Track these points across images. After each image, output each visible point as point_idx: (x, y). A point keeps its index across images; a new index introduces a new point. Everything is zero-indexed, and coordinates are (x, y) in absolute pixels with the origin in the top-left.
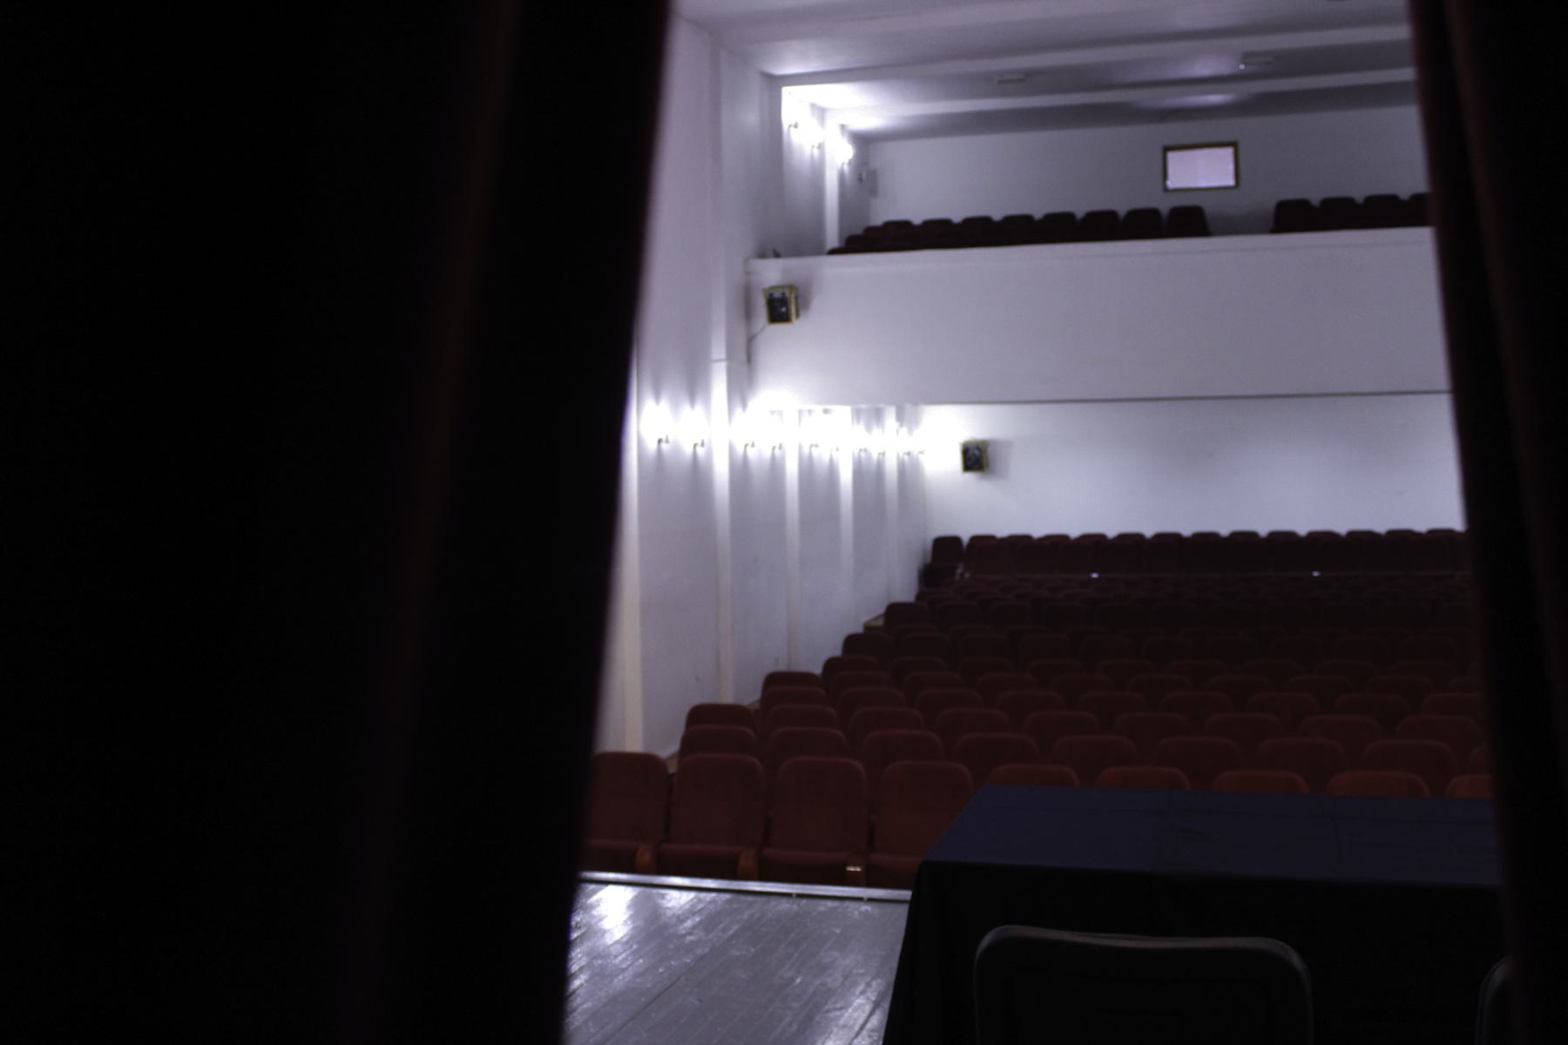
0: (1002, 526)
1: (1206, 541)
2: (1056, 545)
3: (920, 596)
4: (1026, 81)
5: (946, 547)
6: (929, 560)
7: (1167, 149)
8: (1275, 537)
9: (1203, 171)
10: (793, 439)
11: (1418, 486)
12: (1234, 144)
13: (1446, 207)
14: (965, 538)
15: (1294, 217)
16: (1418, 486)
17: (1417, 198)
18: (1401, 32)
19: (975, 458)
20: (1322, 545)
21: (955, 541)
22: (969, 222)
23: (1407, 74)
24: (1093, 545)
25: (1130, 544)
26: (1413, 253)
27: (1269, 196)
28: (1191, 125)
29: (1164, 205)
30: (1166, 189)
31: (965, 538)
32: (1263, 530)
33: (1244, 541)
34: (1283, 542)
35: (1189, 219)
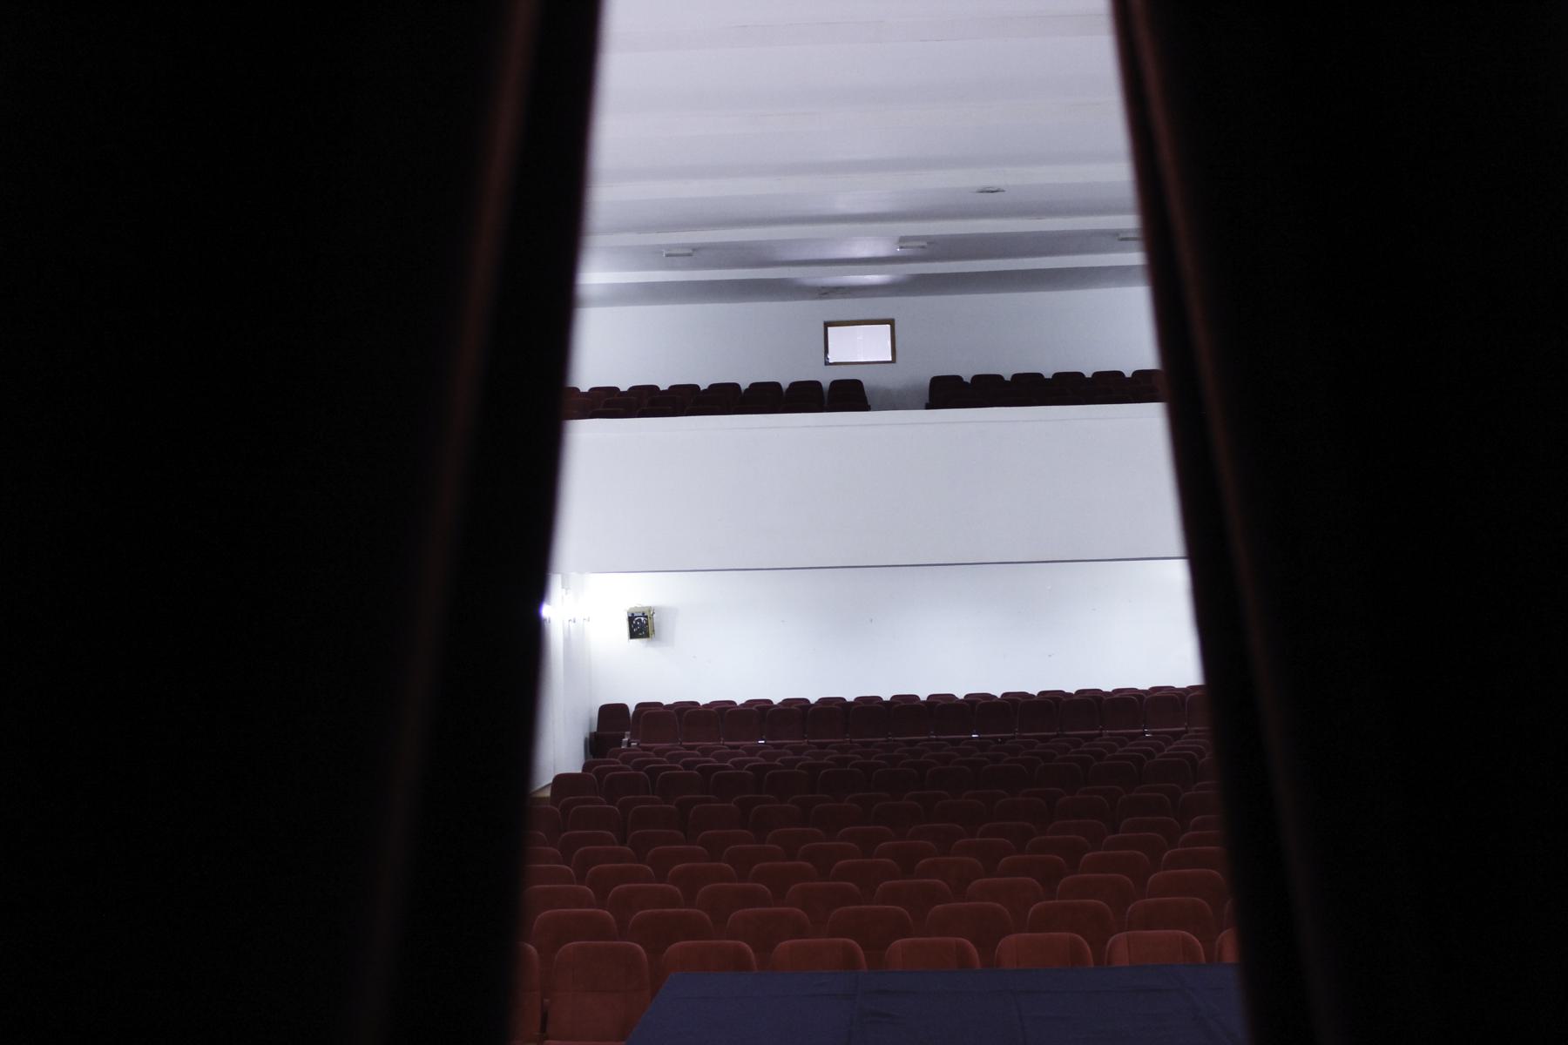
0: (668, 695)
1: (868, 705)
2: (722, 712)
3: (586, 767)
4: (693, 255)
5: (612, 715)
6: (595, 729)
7: (827, 325)
8: (972, 699)
9: (860, 347)
10: (667, 591)
11: (1138, 632)
12: (891, 322)
13: (1174, 383)
14: (1128, 374)
15: (948, 392)
16: (1138, 632)
17: (1140, 375)
18: (1129, 221)
19: (640, 627)
20: (979, 705)
21: (622, 708)
22: (637, 391)
23: (1135, 258)
24: (759, 712)
25: (796, 709)
26: (1145, 427)
27: (922, 372)
28: (841, 299)
29: (826, 378)
30: (827, 363)
31: (1128, 374)
32: (1071, 688)
33: (905, 705)
34: (942, 705)
35: (847, 395)
